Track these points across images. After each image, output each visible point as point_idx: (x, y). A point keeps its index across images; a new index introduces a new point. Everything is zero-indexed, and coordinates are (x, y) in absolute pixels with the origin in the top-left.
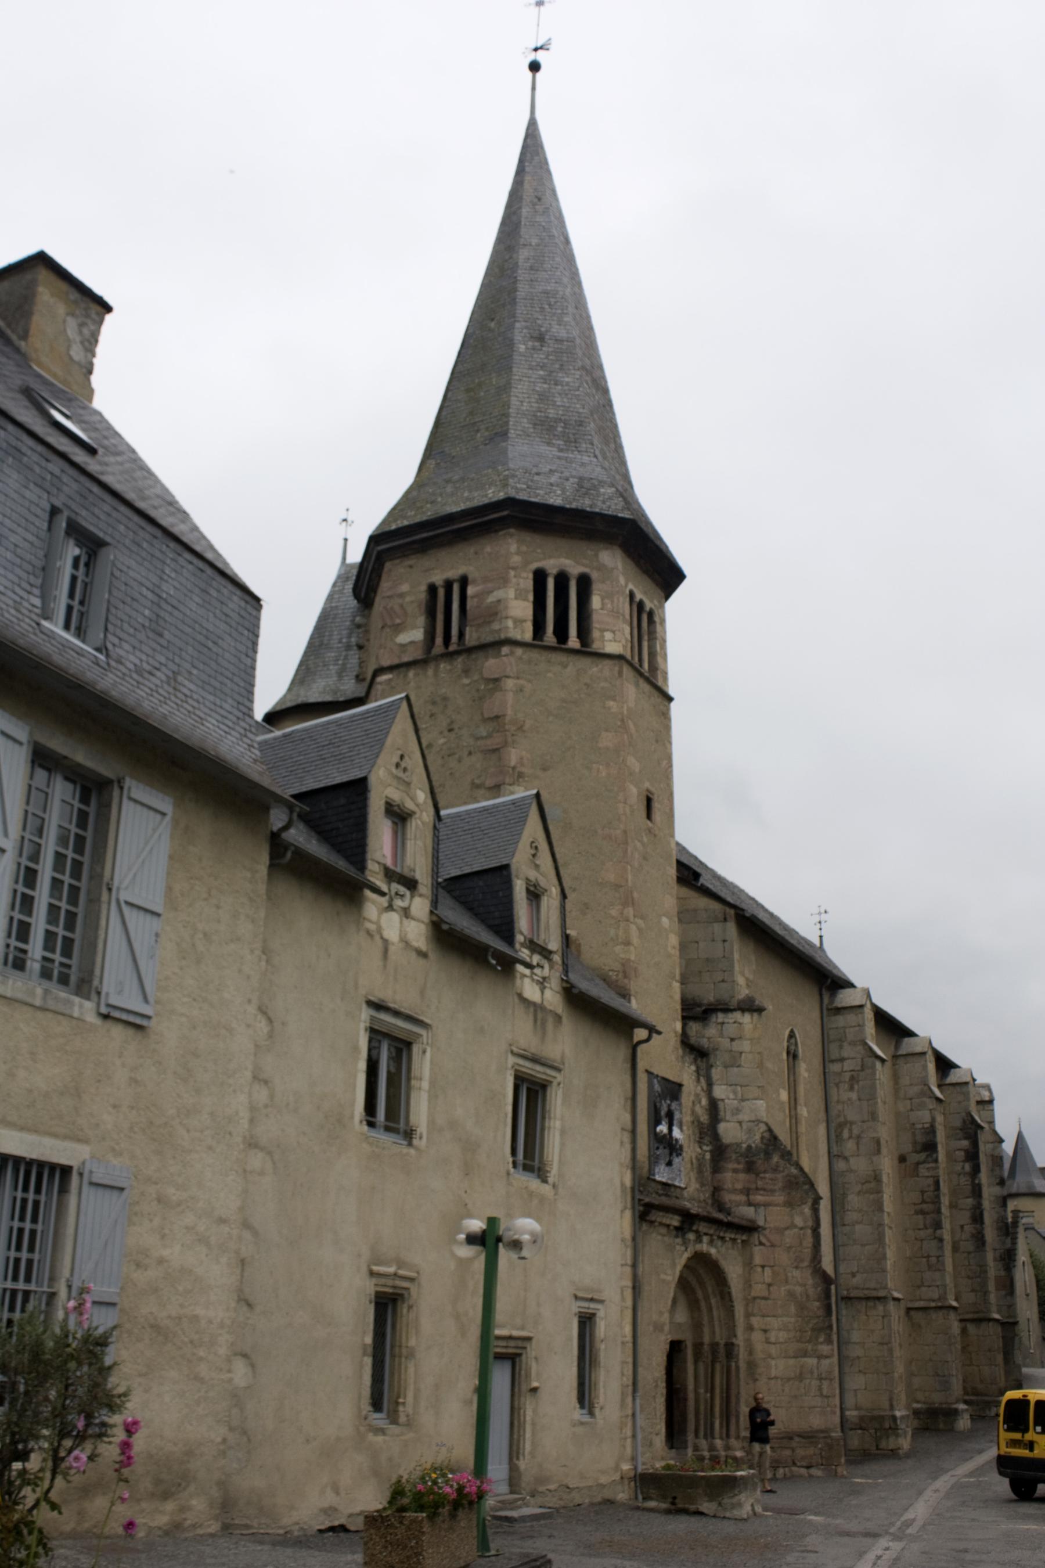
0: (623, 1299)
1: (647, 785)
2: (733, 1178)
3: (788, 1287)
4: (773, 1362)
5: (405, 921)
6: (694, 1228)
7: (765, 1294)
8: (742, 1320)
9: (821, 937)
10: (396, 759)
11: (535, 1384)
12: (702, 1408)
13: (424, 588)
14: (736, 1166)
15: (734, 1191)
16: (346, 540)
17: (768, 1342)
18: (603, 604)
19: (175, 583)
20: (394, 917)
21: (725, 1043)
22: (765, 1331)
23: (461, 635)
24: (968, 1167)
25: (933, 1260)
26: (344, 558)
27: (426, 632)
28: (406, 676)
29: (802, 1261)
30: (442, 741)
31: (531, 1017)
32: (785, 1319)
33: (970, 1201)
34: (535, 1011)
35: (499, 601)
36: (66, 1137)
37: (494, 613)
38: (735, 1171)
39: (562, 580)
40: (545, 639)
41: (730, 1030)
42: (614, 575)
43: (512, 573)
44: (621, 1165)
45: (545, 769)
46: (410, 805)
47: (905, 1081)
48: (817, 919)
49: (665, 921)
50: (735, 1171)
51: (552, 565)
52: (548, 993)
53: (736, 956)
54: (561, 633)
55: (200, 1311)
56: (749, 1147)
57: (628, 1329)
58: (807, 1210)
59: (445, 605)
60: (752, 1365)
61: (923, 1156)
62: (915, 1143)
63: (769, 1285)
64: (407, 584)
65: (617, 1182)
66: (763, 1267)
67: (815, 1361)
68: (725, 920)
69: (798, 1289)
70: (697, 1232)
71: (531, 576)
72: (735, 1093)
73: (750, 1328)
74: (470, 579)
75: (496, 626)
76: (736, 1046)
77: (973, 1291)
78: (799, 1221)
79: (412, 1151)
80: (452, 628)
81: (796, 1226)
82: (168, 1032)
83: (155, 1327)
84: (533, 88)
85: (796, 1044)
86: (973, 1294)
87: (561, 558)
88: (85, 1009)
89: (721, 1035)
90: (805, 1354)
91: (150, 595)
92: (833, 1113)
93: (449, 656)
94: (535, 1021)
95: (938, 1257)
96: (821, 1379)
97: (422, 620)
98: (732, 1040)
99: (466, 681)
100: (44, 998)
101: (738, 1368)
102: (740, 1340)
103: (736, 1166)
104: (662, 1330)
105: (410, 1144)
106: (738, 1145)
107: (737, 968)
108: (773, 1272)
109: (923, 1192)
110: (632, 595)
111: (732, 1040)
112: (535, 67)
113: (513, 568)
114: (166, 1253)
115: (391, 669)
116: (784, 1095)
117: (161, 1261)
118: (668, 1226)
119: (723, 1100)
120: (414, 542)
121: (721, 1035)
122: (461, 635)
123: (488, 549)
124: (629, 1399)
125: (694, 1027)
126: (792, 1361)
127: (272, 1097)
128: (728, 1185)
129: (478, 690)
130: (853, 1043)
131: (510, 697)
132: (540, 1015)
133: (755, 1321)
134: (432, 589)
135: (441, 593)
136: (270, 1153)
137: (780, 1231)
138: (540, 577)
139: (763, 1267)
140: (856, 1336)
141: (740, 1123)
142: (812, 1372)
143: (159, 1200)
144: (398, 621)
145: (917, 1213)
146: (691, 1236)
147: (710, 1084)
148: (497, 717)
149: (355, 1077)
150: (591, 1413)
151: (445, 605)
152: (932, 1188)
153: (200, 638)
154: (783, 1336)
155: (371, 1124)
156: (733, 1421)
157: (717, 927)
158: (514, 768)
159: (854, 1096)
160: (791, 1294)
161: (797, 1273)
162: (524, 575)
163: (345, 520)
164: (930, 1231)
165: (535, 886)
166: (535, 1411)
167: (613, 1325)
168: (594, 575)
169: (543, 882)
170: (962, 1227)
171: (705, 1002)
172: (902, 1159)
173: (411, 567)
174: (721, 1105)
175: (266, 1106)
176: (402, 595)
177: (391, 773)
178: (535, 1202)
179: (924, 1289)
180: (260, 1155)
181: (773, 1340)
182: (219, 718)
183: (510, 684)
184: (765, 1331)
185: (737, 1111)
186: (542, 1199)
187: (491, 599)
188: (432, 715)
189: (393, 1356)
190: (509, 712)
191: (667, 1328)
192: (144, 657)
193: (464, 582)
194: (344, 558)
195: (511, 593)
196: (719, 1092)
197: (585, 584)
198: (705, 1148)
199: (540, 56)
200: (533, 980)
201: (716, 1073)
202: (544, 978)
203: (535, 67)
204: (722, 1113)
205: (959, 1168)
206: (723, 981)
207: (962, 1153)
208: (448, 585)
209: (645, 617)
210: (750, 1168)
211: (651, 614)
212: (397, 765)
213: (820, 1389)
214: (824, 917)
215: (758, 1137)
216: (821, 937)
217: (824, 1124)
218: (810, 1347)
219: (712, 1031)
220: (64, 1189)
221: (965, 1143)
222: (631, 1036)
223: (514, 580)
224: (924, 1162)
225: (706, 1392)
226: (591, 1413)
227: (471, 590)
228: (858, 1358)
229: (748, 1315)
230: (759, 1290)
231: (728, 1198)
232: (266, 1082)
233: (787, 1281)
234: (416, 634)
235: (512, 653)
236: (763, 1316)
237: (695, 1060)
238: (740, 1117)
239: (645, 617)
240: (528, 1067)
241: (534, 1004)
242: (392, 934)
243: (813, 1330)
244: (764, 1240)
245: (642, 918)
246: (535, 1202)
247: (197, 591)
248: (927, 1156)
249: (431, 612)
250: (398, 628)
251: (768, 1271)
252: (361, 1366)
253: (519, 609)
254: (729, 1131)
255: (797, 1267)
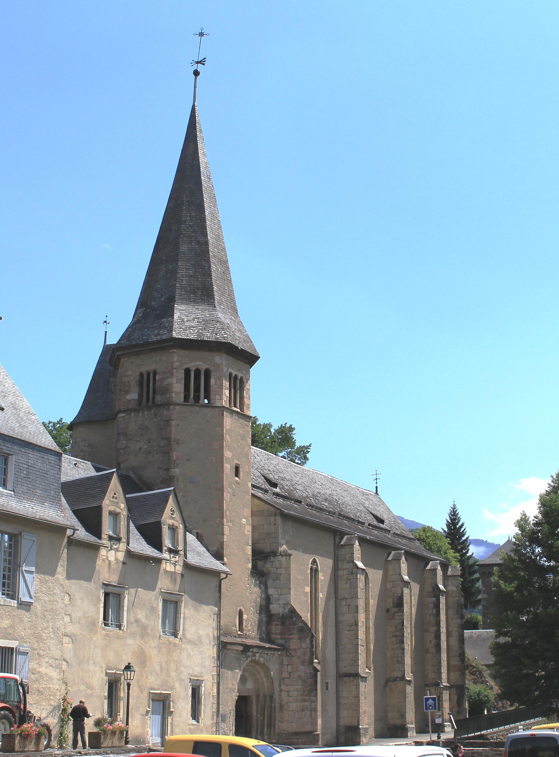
0: (213, 679)
1: (236, 462)
2: (276, 628)
3: (298, 673)
4: (291, 704)
5: (117, 553)
6: (251, 650)
7: (288, 676)
8: (278, 687)
9: (377, 487)
10: (112, 494)
11: (172, 710)
12: (259, 722)
13: (138, 374)
14: (277, 623)
15: (276, 634)
16: (106, 332)
17: (289, 696)
18: (216, 382)
19: (34, 459)
20: (113, 552)
21: (273, 570)
22: (288, 692)
23: (154, 398)
24: (434, 611)
25: (400, 659)
26: (105, 342)
27: (139, 395)
28: (130, 415)
29: (305, 662)
30: (145, 447)
31: (170, 578)
32: (297, 687)
33: (434, 628)
34: (172, 575)
35: (169, 384)
36: (12, 640)
37: (167, 390)
38: (277, 625)
39: (197, 372)
40: (190, 401)
41: (277, 564)
42: (225, 364)
43: (175, 371)
44: (213, 628)
45: (188, 460)
46: (118, 510)
47: (391, 573)
48: (375, 477)
49: (244, 520)
50: (277, 625)
51: (193, 366)
52: (178, 567)
53: (280, 531)
54: (197, 398)
55: (51, 686)
56: (283, 615)
57: (215, 691)
58: (308, 641)
59: (147, 382)
60: (281, 706)
61: (397, 609)
62: (393, 603)
63: (290, 673)
64: (132, 369)
65: (211, 635)
66: (288, 665)
67: (309, 703)
68: (276, 515)
69: (303, 674)
70: (252, 652)
71: (183, 371)
72: (277, 591)
73: (281, 691)
74: (157, 372)
75: (168, 396)
76: (279, 571)
77: (434, 672)
78: (304, 646)
79: (121, 632)
80: (150, 391)
81: (303, 648)
82: (38, 607)
83: (39, 691)
84: (195, 87)
85: (317, 565)
86: (434, 674)
87: (197, 362)
88: (14, 603)
89: (272, 566)
90: (305, 700)
91: (25, 466)
92: (340, 592)
93: (149, 408)
94: (172, 578)
95: (402, 657)
96: (311, 711)
97: (137, 389)
98: (277, 569)
99: (156, 420)
100: (4, 602)
101: (275, 706)
102: (276, 696)
103: (277, 623)
104: (234, 692)
105: (120, 629)
106: (279, 614)
107: (280, 536)
108: (292, 667)
109: (396, 627)
110: (230, 374)
111: (277, 569)
112: (196, 73)
113: (175, 369)
114: (40, 670)
115: (124, 412)
116: (308, 589)
117: (39, 672)
118: (237, 650)
119: (272, 595)
120: (134, 352)
121: (272, 566)
122: (154, 398)
123: (165, 359)
124: (215, 717)
125: (260, 563)
126: (299, 704)
127: (71, 620)
128: (273, 631)
129: (160, 425)
130: (348, 562)
131: (173, 429)
132: (173, 576)
133: (283, 687)
134: (141, 374)
135: (145, 377)
136: (71, 637)
137: (295, 650)
138: (187, 372)
139: (288, 665)
140: (345, 694)
141: (279, 604)
142: (307, 708)
143: (38, 654)
144: (127, 389)
145: (393, 636)
146: (250, 654)
147: (266, 588)
148: (168, 438)
149: (99, 609)
150: (198, 722)
151: (147, 382)
152: (400, 625)
153: (42, 474)
154: (296, 693)
155: (106, 625)
156: (273, 728)
157: (272, 519)
158: (175, 461)
159: (348, 586)
160: (299, 676)
161: (302, 667)
162: (180, 371)
163: (105, 322)
164: (398, 645)
165: (172, 526)
166: (172, 719)
167: (208, 689)
168: (212, 368)
169: (176, 524)
170: (430, 641)
171: (266, 552)
172: (388, 611)
173: (132, 363)
174: (271, 597)
175: (69, 623)
176: (128, 376)
177: (110, 500)
178: (172, 645)
179: (395, 672)
180: (68, 638)
181: (291, 695)
182: (50, 500)
183: (173, 423)
184: (288, 692)
185: (278, 600)
186: (175, 644)
187: (166, 382)
188: (142, 435)
189: (115, 699)
190: (173, 436)
191: (236, 690)
192: (25, 488)
193: (155, 373)
194: (105, 342)
195: (174, 380)
196: (271, 591)
197: (208, 373)
198: (263, 616)
199: (200, 68)
200: (171, 563)
201: (270, 583)
202: (176, 562)
203: (196, 73)
204: (271, 601)
205: (430, 612)
206: (274, 543)
207: (432, 604)
208: (148, 374)
209: (238, 382)
210: (283, 623)
211: (241, 380)
212: (113, 497)
213: (311, 715)
214: (378, 476)
215: (287, 611)
216: (377, 487)
217: (334, 599)
218: (307, 698)
219: (268, 565)
220: (12, 654)
221: (434, 599)
222: (219, 576)
223: (176, 374)
224: (397, 612)
225: (261, 716)
226: (198, 722)
227: (157, 377)
228: (346, 703)
229: (280, 685)
230: (285, 675)
231: (273, 636)
232: (69, 615)
233: (298, 671)
234: (133, 396)
235: (175, 409)
236: (287, 685)
237: (259, 578)
238: (280, 602)
239: (238, 382)
240: (168, 597)
241: (171, 572)
242: (112, 558)
243: (309, 691)
244: (288, 654)
245: (231, 522)
246: (172, 645)
247: (40, 458)
248: (399, 610)
249: (141, 384)
250: (127, 392)
251: (290, 667)
252: (104, 702)
253: (178, 387)
254: (275, 608)
255: (302, 665)
